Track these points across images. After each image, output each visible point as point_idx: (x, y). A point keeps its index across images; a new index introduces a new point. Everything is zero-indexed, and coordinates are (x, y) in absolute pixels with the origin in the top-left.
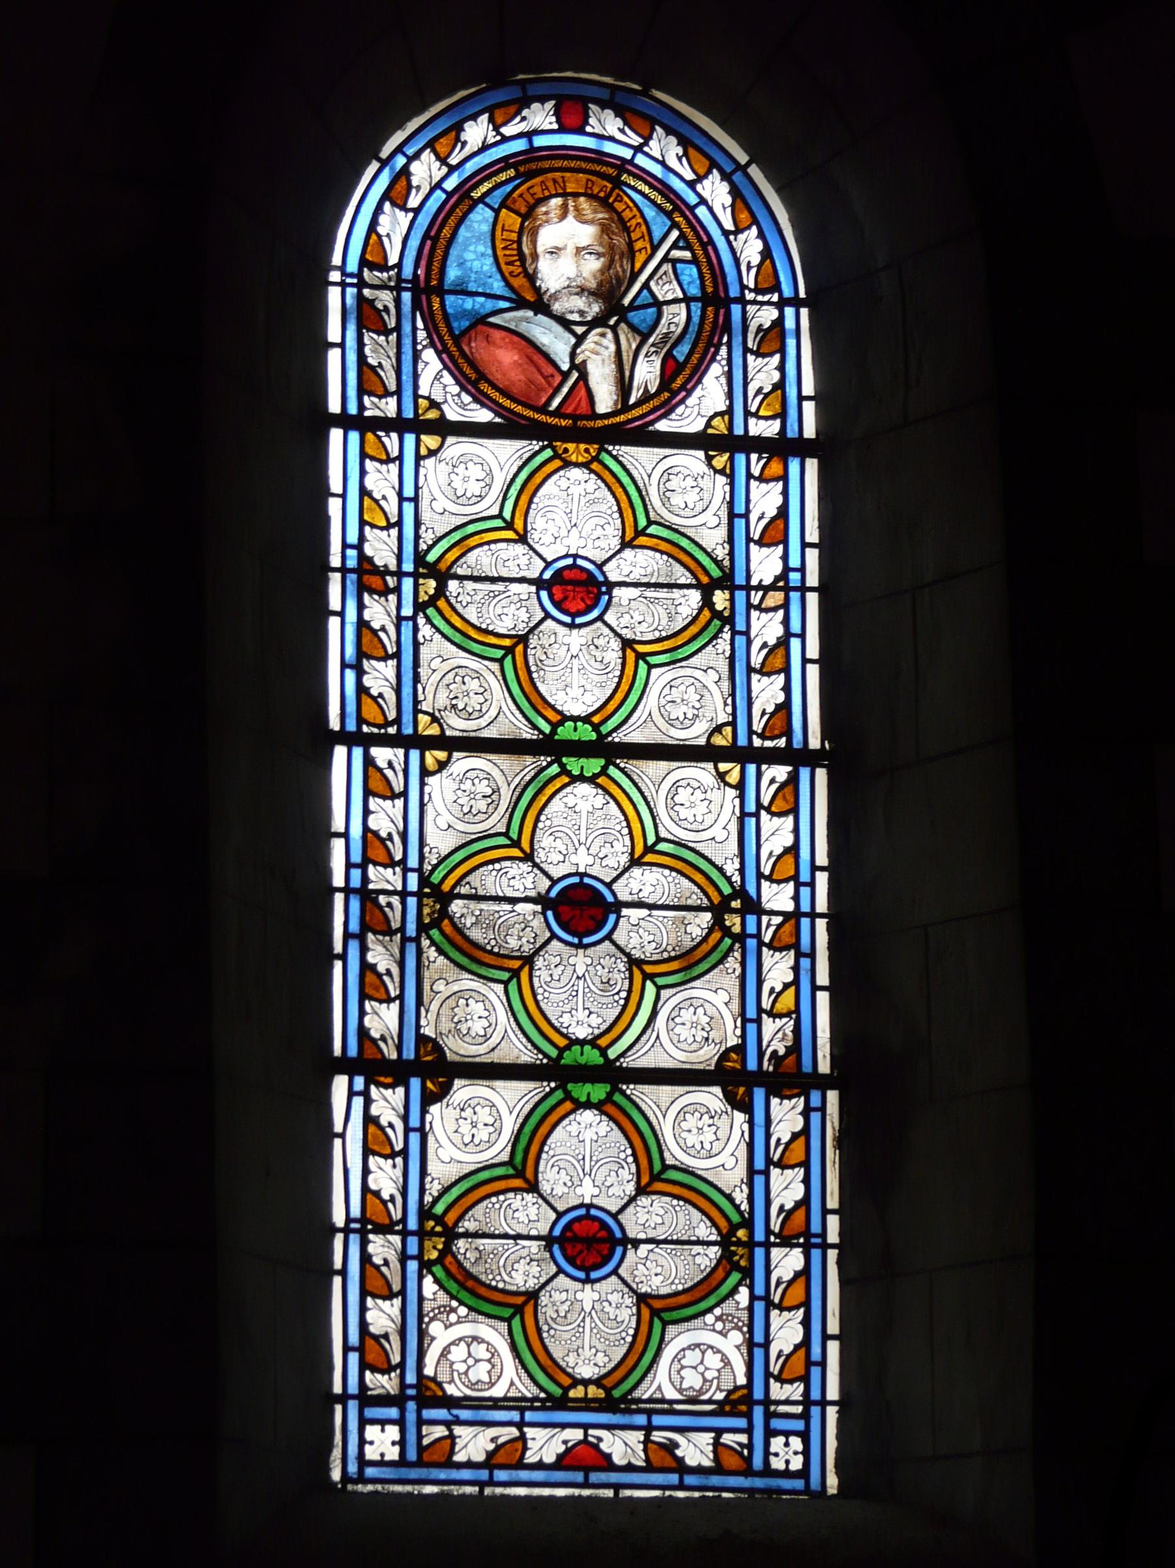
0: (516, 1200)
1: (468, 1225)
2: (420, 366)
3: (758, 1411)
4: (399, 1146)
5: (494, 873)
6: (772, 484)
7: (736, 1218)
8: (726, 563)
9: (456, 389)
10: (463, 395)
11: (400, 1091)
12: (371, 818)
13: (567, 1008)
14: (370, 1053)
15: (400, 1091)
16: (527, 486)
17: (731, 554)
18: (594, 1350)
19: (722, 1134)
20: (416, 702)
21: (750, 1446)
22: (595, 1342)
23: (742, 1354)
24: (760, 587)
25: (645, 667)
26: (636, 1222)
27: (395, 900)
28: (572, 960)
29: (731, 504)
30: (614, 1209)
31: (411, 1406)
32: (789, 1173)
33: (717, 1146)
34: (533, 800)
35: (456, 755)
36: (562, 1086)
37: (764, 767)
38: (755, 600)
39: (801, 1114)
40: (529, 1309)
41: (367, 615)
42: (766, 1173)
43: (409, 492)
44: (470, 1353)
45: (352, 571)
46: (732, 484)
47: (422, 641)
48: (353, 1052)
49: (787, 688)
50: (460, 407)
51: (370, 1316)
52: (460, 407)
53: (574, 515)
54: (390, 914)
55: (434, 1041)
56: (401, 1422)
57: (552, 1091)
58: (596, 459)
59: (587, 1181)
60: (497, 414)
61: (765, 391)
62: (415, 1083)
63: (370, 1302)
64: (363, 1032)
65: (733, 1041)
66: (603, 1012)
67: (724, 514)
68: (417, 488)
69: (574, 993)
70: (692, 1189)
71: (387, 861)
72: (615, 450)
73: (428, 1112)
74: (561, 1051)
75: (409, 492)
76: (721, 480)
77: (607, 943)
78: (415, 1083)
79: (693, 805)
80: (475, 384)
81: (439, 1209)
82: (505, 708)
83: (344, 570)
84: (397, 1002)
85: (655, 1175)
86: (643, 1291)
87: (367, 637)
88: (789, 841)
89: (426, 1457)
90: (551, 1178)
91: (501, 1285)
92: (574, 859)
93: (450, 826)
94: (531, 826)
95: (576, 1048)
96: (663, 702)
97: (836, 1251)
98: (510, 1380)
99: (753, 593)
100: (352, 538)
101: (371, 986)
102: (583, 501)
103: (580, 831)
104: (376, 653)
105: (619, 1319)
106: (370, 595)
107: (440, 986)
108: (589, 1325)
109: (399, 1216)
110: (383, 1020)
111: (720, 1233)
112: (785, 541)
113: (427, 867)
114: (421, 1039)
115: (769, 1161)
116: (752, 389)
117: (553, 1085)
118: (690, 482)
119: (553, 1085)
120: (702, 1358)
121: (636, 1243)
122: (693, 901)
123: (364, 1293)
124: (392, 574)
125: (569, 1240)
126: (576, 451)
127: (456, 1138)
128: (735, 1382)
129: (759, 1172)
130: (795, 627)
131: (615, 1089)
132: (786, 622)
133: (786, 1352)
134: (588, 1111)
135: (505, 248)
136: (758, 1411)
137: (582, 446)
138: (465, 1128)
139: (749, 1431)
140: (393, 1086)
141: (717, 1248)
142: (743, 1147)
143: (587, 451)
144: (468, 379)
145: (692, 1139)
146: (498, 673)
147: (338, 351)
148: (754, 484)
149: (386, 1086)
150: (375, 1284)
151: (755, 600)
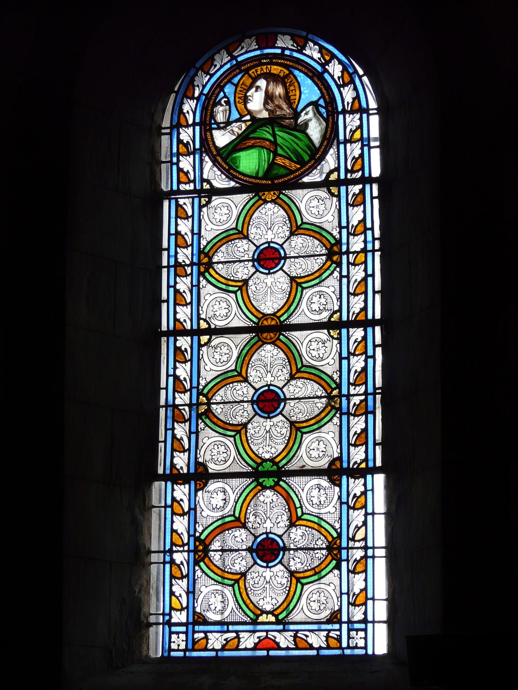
0: (238, 386)
1: (218, 398)
2: (204, 163)
3: (345, 627)
4: (188, 301)
5: (231, 245)
6: (359, 236)
7: (333, 241)
8: (339, 530)
9: (219, 173)
10: (223, 175)
11: (187, 486)
12: (175, 492)
13: (262, 597)
14: (179, 326)
15: (187, 486)
16: (247, 215)
17: (340, 377)
18: (270, 447)
19: (328, 207)
20: (199, 314)
21: (340, 636)
22: (272, 594)
23: (333, 158)
24: (354, 253)
25: (300, 434)
26: (290, 391)
27: (187, 408)
28: (265, 424)
29: (340, 354)
30: (281, 386)
31: (190, 627)
32: (357, 268)
33: (326, 356)
34: (248, 499)
35: (213, 337)
36: (257, 480)
37: (349, 187)
38: (351, 260)
39: (363, 271)
40: (243, 431)
41: (179, 228)
42: (348, 359)
43: (196, 231)
44: (215, 600)
45: (172, 266)
46: (340, 343)
47: (338, 372)
48: (168, 472)
49: (364, 212)
50: (220, 182)
51: (175, 461)
52: (220, 182)
53: (269, 224)
54: (185, 414)
55: (200, 613)
56: (186, 633)
57: (254, 337)
58: (278, 197)
59: (268, 521)
60: (237, 182)
61: (359, 340)
62: (193, 483)
63: (178, 364)
64: (176, 320)
65: (336, 455)
66: (277, 447)
67: (337, 357)
68: (195, 505)
69: (265, 589)
70: (315, 375)
71: (187, 181)
72: (287, 192)
73: (202, 211)
74: (259, 465)
75: (196, 231)
76: (336, 342)
77: (280, 565)
78: (193, 483)
79: (318, 349)
80: (228, 171)
81: (205, 391)
82: (236, 458)
83: (168, 267)
84: (186, 610)
85: (299, 370)
86: (292, 570)
87: (179, 296)
88: (363, 426)
89: (196, 647)
90: (253, 374)
91: (232, 278)
92: (266, 237)
93: (211, 369)
94: (247, 446)
95: (264, 615)
96: (308, 450)
97: (380, 396)
98: (232, 611)
99: (347, 115)
100: (172, 283)
101: (177, 446)
102: (273, 217)
103: (269, 514)
104: (183, 216)
105: (282, 433)
106: (182, 156)
107: (203, 589)
108: (268, 585)
109: (189, 358)
110: (184, 313)
111: (326, 248)
112: (366, 443)
113: (201, 387)
114: (197, 463)
115: (349, 353)
116: (352, 433)
117: (254, 334)
118: (320, 344)
119: (254, 334)
120: (319, 599)
121: (290, 549)
122: (319, 393)
123: (173, 450)
124: (188, 266)
125: (263, 259)
126: (269, 196)
127: (213, 361)
128: (330, 167)
129: (345, 358)
130: (370, 272)
131: (280, 480)
132: (365, 270)
133: (355, 225)
134: (268, 490)
135: (240, 91)
136: (345, 627)
137: (272, 193)
138: (217, 356)
139: (340, 630)
140: (184, 484)
141: (325, 399)
142: (337, 211)
143: (274, 194)
144: (224, 168)
145: (314, 353)
146: (235, 299)
147: (166, 304)
148: (352, 448)
149: (181, 484)
150: (180, 241)
151: (351, 260)
